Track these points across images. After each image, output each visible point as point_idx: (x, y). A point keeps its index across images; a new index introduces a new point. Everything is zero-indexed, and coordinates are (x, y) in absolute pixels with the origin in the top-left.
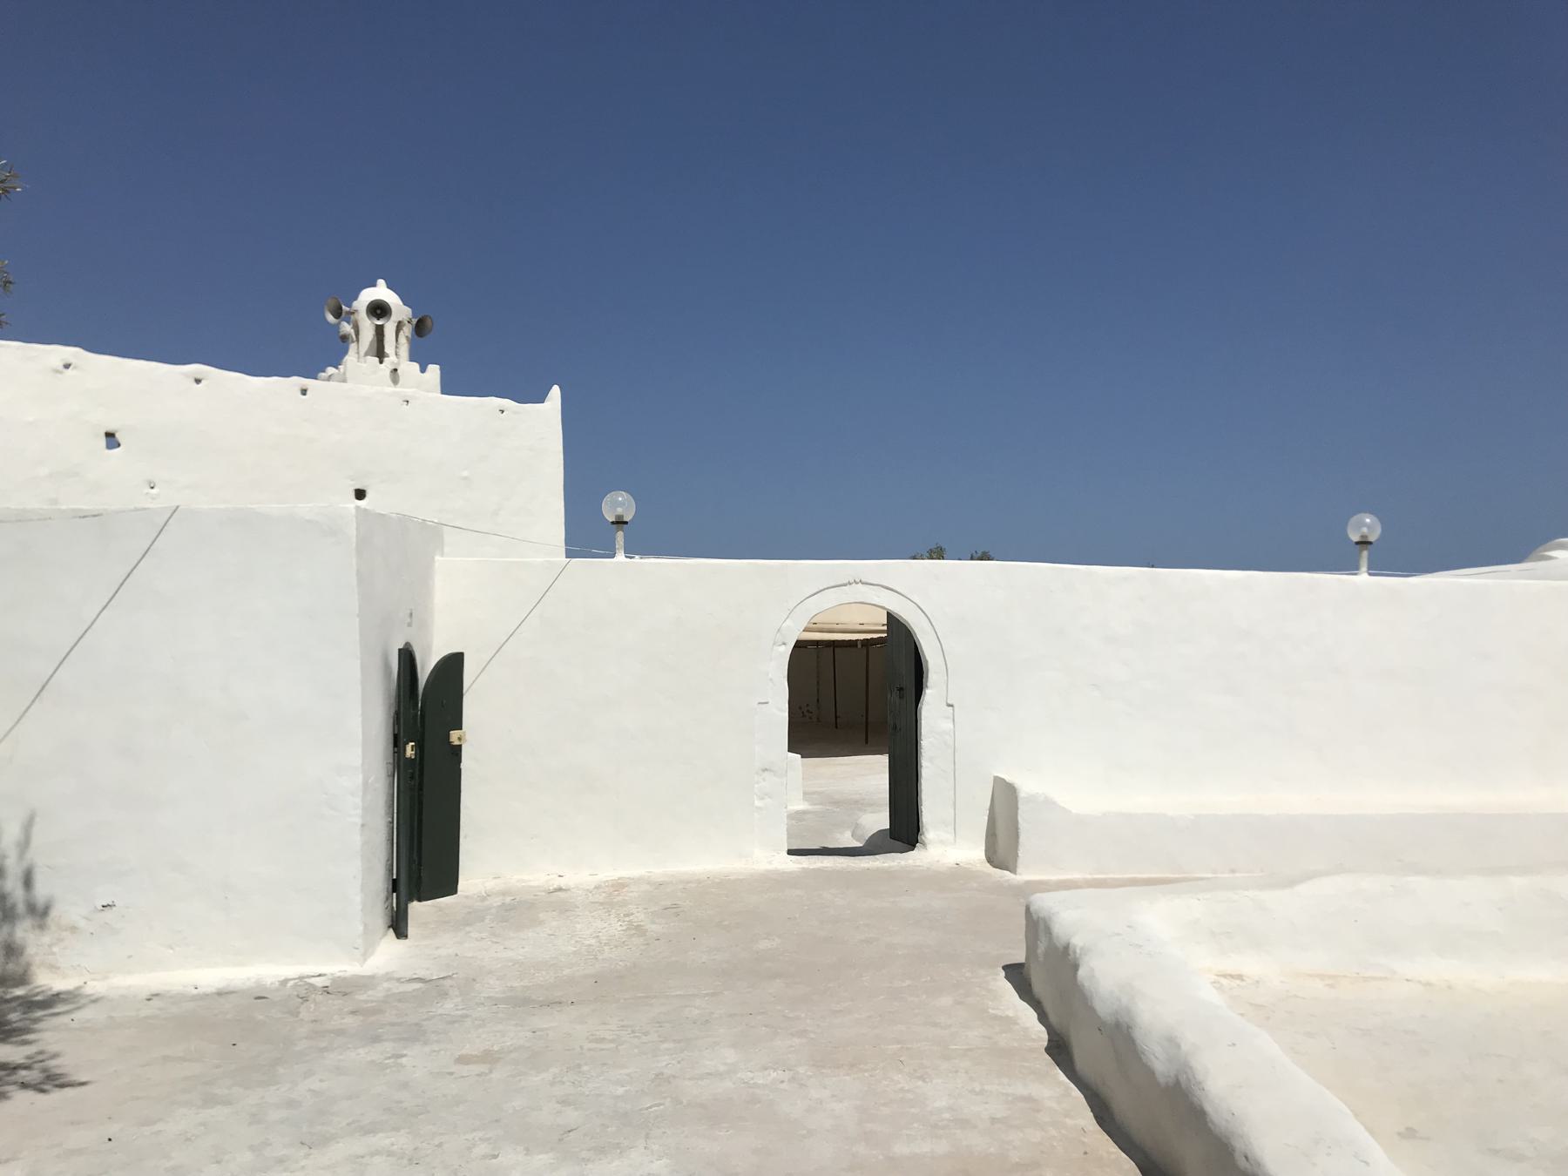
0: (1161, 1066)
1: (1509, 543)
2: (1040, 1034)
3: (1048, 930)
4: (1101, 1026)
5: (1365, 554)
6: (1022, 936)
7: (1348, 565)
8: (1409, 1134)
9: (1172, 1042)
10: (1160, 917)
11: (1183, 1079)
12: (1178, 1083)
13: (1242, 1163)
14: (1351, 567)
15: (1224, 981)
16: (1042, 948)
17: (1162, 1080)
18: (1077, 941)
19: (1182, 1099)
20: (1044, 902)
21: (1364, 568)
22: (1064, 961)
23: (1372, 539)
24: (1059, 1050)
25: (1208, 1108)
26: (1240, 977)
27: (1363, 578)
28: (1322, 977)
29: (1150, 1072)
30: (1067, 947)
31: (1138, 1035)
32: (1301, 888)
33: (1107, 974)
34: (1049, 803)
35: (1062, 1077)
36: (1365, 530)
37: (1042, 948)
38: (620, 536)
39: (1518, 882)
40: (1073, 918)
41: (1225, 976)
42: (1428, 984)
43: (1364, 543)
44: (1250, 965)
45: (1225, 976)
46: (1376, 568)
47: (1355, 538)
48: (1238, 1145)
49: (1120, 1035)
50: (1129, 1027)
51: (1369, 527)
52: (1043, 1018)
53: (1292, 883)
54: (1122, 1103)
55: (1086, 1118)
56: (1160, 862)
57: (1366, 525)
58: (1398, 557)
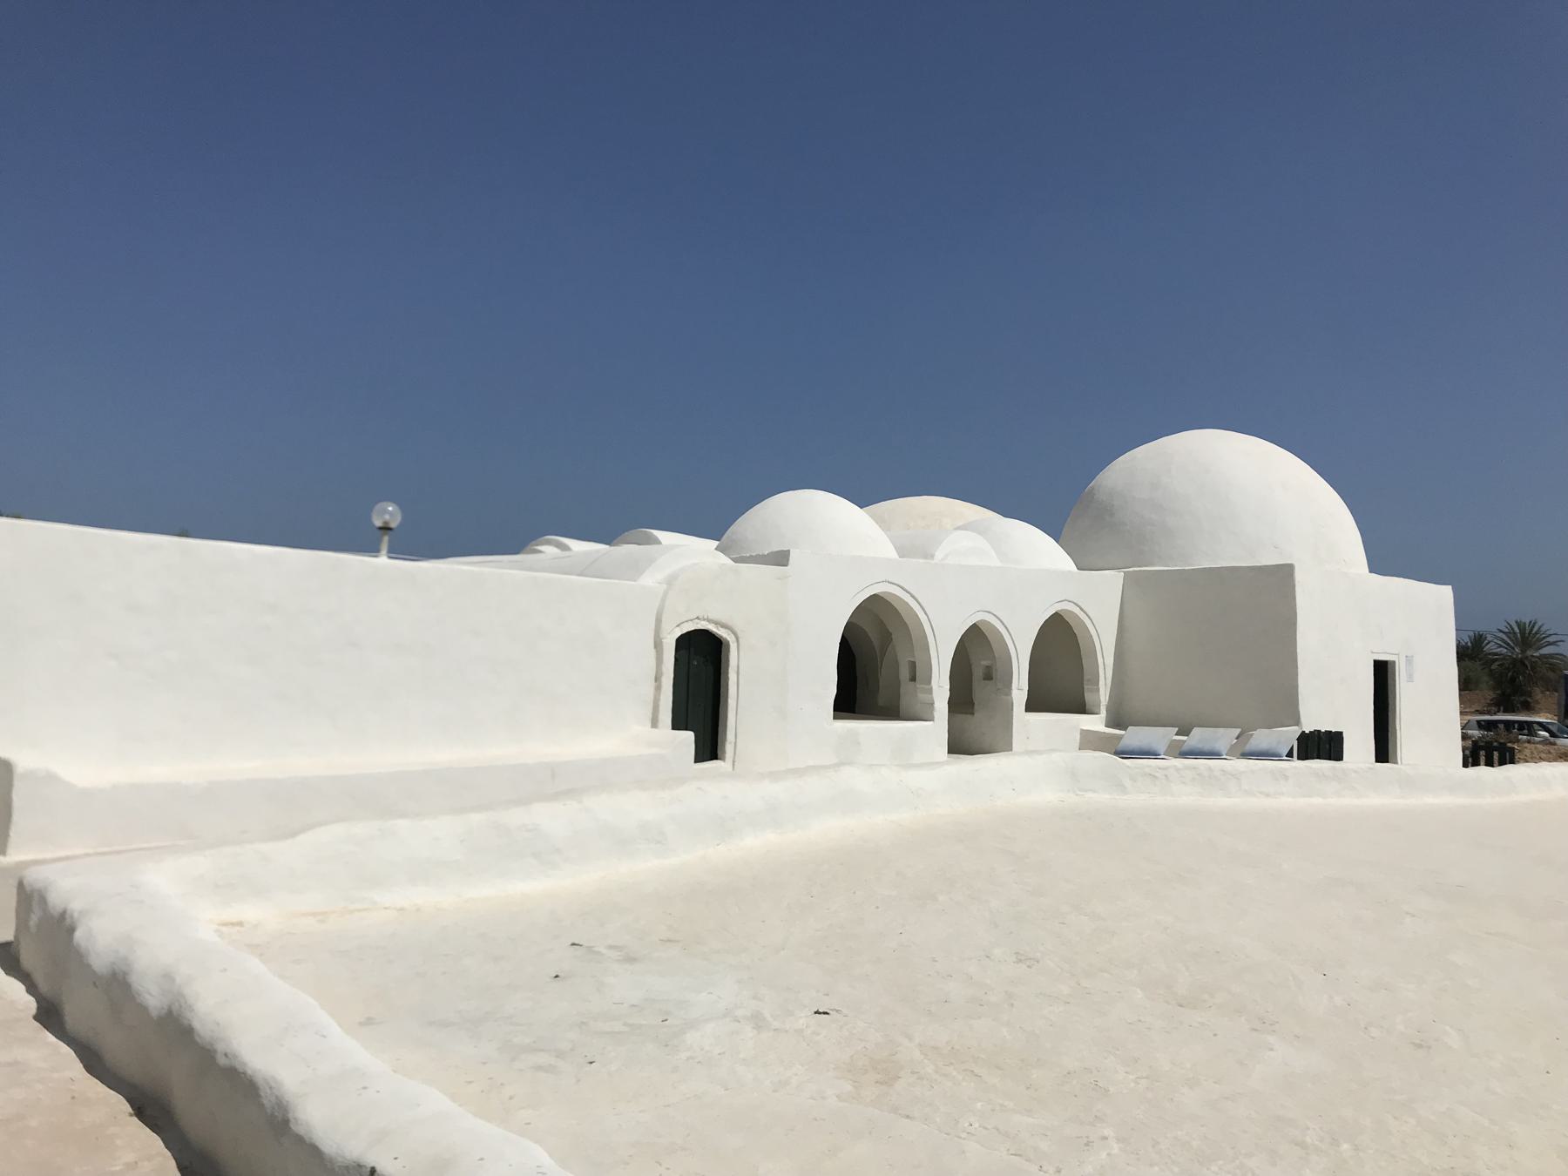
0: (154, 999)
1: (507, 536)
2: (30, 1004)
3: (43, 900)
4: (95, 979)
5: (386, 538)
6: (12, 915)
7: (369, 547)
8: (369, 1021)
9: (168, 977)
10: (163, 878)
11: (175, 1008)
12: (170, 1012)
13: (222, 1061)
14: (373, 550)
15: (224, 929)
16: (34, 920)
17: (154, 1013)
18: (75, 906)
19: (175, 1028)
20: (34, 876)
21: (384, 552)
22: (59, 928)
23: (393, 525)
24: (50, 1016)
25: (196, 1025)
26: (240, 924)
27: (383, 560)
28: (314, 914)
29: (143, 1009)
30: (63, 915)
31: (134, 980)
32: (301, 838)
33: (102, 935)
34: (51, 778)
35: (51, 1038)
36: (387, 517)
37: (34, 920)
38: (386, 538)
39: (476, 818)
40: (67, 888)
41: (225, 924)
42: (402, 909)
43: (386, 529)
44: (250, 912)
45: (225, 924)
46: (396, 552)
47: (378, 523)
48: (220, 1047)
49: (117, 985)
50: (125, 974)
51: (391, 513)
52: (32, 988)
53: (294, 834)
54: (114, 1045)
55: (76, 1068)
56: (172, 819)
57: (389, 513)
58: (414, 543)
